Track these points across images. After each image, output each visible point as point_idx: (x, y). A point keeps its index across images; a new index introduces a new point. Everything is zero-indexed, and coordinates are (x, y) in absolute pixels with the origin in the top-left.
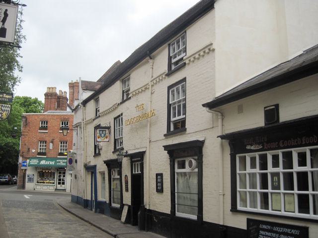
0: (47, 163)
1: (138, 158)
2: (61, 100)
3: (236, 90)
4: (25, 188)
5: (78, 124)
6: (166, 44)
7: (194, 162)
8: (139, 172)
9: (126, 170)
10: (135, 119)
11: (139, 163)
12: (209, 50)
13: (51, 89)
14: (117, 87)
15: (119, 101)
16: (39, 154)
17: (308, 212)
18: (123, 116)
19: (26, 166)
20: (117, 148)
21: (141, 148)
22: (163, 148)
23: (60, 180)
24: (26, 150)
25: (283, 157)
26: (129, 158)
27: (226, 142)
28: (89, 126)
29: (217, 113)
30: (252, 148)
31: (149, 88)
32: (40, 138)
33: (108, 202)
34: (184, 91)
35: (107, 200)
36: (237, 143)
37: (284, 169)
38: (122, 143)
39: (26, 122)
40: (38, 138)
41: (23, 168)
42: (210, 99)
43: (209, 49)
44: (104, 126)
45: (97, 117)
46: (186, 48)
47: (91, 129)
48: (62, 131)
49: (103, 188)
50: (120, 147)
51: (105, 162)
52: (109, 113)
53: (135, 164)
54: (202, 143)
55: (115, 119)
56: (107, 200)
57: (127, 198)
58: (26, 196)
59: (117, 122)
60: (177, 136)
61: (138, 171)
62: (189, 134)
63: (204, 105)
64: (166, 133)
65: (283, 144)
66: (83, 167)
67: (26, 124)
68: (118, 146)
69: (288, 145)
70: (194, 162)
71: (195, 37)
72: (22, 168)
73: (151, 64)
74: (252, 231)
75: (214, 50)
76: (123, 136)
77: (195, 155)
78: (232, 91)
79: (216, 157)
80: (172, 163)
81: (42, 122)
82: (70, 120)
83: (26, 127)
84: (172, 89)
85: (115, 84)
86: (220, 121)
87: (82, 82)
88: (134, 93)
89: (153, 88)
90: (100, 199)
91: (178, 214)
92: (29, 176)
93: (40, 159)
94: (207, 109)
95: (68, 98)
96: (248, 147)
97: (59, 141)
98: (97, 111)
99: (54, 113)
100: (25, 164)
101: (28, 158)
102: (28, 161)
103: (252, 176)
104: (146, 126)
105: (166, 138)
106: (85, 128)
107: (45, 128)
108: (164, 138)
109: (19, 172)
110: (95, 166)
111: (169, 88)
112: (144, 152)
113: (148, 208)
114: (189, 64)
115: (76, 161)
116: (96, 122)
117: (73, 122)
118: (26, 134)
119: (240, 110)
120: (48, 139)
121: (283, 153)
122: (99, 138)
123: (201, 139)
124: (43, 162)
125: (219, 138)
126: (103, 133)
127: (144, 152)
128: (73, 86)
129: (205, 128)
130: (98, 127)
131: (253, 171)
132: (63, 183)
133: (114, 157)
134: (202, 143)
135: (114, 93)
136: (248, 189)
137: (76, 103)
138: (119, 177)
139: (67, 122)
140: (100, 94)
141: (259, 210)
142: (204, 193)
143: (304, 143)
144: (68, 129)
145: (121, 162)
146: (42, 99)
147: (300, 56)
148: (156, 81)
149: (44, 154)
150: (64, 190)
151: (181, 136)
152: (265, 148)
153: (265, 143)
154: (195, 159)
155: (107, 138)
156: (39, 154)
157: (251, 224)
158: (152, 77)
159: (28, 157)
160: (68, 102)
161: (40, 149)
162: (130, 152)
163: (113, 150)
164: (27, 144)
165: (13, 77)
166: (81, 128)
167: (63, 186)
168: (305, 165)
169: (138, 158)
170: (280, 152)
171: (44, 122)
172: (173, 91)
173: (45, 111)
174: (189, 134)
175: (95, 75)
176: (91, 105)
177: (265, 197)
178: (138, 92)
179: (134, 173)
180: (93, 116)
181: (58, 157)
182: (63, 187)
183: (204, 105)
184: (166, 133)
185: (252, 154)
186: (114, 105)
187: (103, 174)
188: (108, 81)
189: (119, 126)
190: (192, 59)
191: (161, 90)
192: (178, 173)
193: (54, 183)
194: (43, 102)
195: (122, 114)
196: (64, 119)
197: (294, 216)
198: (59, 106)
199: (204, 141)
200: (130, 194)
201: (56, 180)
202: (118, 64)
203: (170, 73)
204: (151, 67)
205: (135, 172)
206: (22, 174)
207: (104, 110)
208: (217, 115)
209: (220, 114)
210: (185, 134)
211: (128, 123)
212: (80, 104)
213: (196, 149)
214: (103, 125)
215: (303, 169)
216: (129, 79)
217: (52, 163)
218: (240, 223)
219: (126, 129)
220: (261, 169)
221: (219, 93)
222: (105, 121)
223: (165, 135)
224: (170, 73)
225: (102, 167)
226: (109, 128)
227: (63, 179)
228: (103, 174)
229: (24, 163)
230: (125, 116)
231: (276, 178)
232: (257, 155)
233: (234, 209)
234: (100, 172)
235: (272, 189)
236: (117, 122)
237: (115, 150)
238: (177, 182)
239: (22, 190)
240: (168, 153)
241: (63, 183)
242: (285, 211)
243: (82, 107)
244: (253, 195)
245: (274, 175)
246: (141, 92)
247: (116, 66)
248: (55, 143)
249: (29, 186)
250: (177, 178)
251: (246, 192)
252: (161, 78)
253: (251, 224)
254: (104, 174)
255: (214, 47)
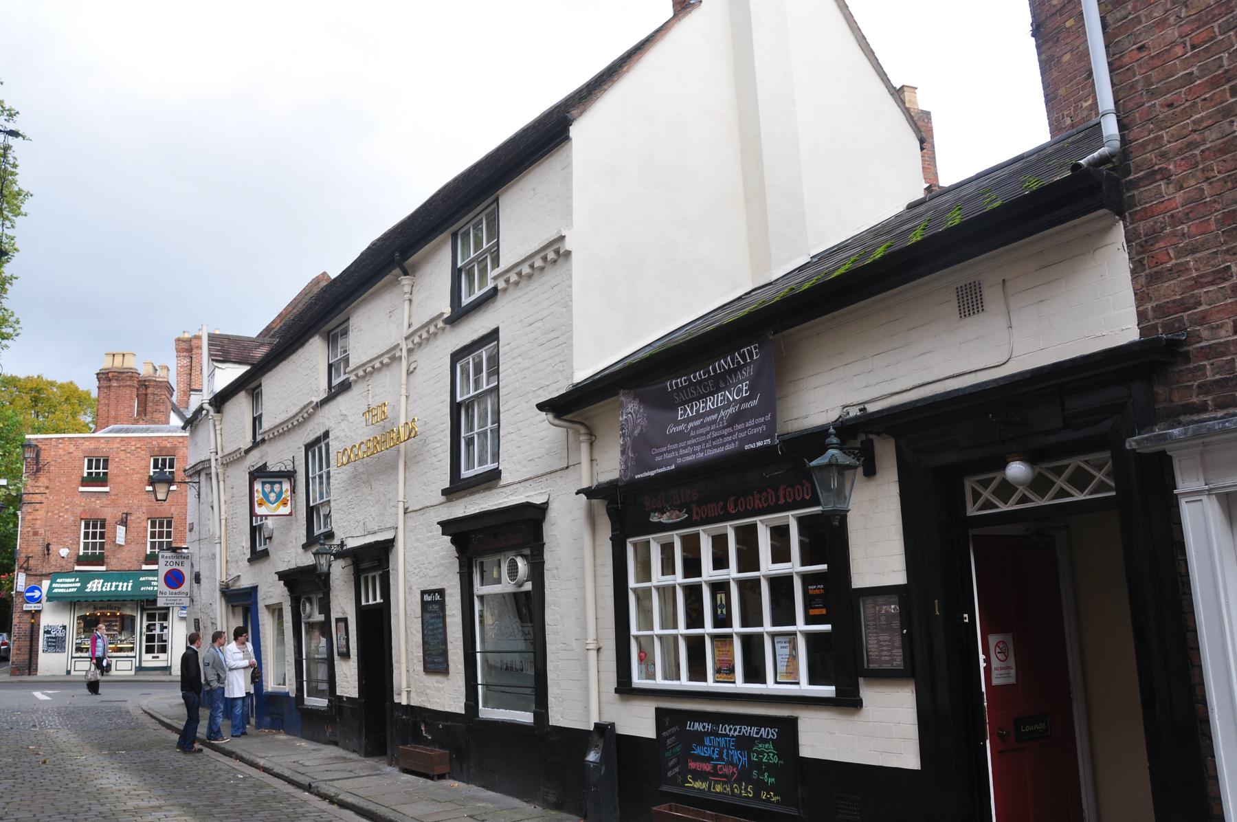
0: (109, 587)
1: (373, 561)
2: (150, 390)
3: (680, 338)
4: (36, 670)
5: (200, 467)
6: (446, 235)
7: (522, 565)
8: (379, 600)
9: (343, 604)
10: (363, 447)
11: (377, 574)
12: (554, 254)
13: (118, 360)
14: (315, 353)
15: (323, 395)
16: (81, 560)
17: (763, 680)
18: (332, 440)
19: (38, 600)
20: (317, 533)
21: (381, 530)
22: (439, 528)
23: (150, 638)
24: (36, 549)
25: (801, 533)
26: (349, 561)
27: (600, 506)
28: (231, 471)
29: (577, 426)
30: (665, 519)
31: (400, 358)
32: (84, 511)
33: (293, 695)
34: (494, 371)
35: (290, 688)
36: (625, 510)
37: (803, 564)
38: (328, 516)
39: (37, 463)
40: (79, 510)
41: (32, 607)
42: (558, 389)
43: (557, 252)
44: (277, 469)
45: (256, 444)
46: (498, 244)
47: (240, 476)
48: (150, 488)
49: (280, 657)
50: (323, 530)
51: (282, 576)
52: (280, 435)
53: (366, 578)
54: (542, 509)
55: (309, 447)
56: (290, 688)
57: (348, 681)
58: (39, 695)
59: (314, 456)
60: (478, 492)
61: (375, 599)
62: (504, 486)
63: (541, 407)
64: (448, 485)
65: (736, 505)
66: (218, 594)
67: (38, 468)
68: (470, 466)
69: (787, 503)
70: (522, 565)
71: (521, 220)
72: (27, 607)
73: (407, 289)
74: (669, 742)
75: (568, 254)
76: (332, 498)
77: (523, 546)
78: (648, 349)
79: (575, 556)
80: (465, 570)
81: (90, 461)
82: (180, 453)
83: (36, 479)
84: (463, 362)
85: (307, 346)
86: (584, 447)
87: (212, 337)
88: (361, 373)
89: (413, 358)
90: (270, 685)
91: (487, 713)
92: (48, 632)
93: (86, 577)
94: (550, 416)
95: (174, 384)
96: (655, 518)
97: (145, 517)
98: (257, 421)
99: (127, 431)
100: (37, 594)
101: (47, 576)
102: (46, 584)
103: (667, 593)
104: (395, 467)
105: (449, 500)
106: (221, 478)
107: (100, 480)
108: (443, 499)
109: (15, 621)
110: (254, 589)
111: (456, 357)
112: (388, 545)
113: (404, 703)
114: (505, 290)
115: (197, 578)
116: (255, 459)
117: (185, 458)
118: (38, 498)
119: (971, 302)
120: (109, 514)
121: (801, 520)
122: (260, 505)
123: (538, 500)
124: (95, 586)
125: (583, 497)
126: (272, 490)
127: (388, 545)
128: (187, 347)
129: (549, 470)
130: (259, 473)
131: (668, 580)
132: (163, 649)
133: (308, 559)
134: (542, 509)
135: (308, 369)
136: (657, 630)
137: (195, 401)
138: (321, 618)
139: (172, 461)
140: (264, 374)
141: (684, 683)
142: (550, 648)
143: (782, 502)
144: (171, 482)
145: (328, 574)
146: (89, 385)
147: (800, 269)
148: (420, 337)
149: (99, 560)
150: (167, 669)
151: (488, 493)
152: (695, 517)
153: (694, 506)
154: (523, 556)
155: (285, 504)
156: (81, 560)
157: (667, 721)
158: (410, 326)
159: (46, 570)
160: (174, 399)
161: (86, 546)
162: (351, 544)
163: (304, 540)
164: (41, 531)
165: (19, 208)
166: (209, 475)
167: (162, 656)
168: (788, 560)
169: (373, 561)
170: (729, 529)
171: (98, 461)
172: (465, 372)
173: (100, 423)
174: (504, 486)
175: (254, 319)
176: (240, 406)
177: (752, 647)
178: (371, 370)
179: (363, 603)
180: (247, 441)
181: (145, 567)
182: (161, 660)
183: (541, 407)
184: (448, 485)
185: (777, 518)
186: (305, 407)
187: (276, 610)
188: (288, 337)
189: (321, 469)
190: (513, 278)
191: (435, 360)
192: (481, 598)
193: (132, 649)
194: (94, 394)
195: (326, 435)
196: (161, 449)
197: (764, 693)
198: (143, 411)
199: (547, 503)
200: (356, 665)
201: (139, 640)
202: (323, 284)
203: (459, 314)
204: (407, 296)
205: (367, 600)
206: (26, 627)
207: (278, 421)
208: (578, 433)
209: (583, 430)
210: (495, 487)
211: (345, 460)
212: (206, 406)
213: (522, 529)
214: (273, 467)
215: (781, 568)
216: (345, 333)
217: (125, 587)
218: (638, 722)
219: (339, 476)
220: (686, 575)
221: (583, 372)
222: (278, 456)
223: (445, 492)
224: (459, 314)
225: (273, 592)
226: (290, 475)
227: (161, 636)
228: (276, 610)
229: (32, 589)
230: (337, 438)
231: (721, 597)
232: (676, 538)
233: (625, 688)
234: (267, 607)
235: (715, 626)
236: (314, 456)
237: (311, 541)
238: (482, 622)
239: (26, 678)
240: (453, 542)
241: (163, 649)
242: (776, 682)
243: (212, 412)
244: (670, 644)
245: (719, 587)
246: (380, 369)
247: (316, 290)
248: (131, 525)
249: (49, 662)
250: (481, 611)
251: (675, 637)
252: (514, 278)
253: (667, 721)
254: (281, 610)
255: (568, 245)
